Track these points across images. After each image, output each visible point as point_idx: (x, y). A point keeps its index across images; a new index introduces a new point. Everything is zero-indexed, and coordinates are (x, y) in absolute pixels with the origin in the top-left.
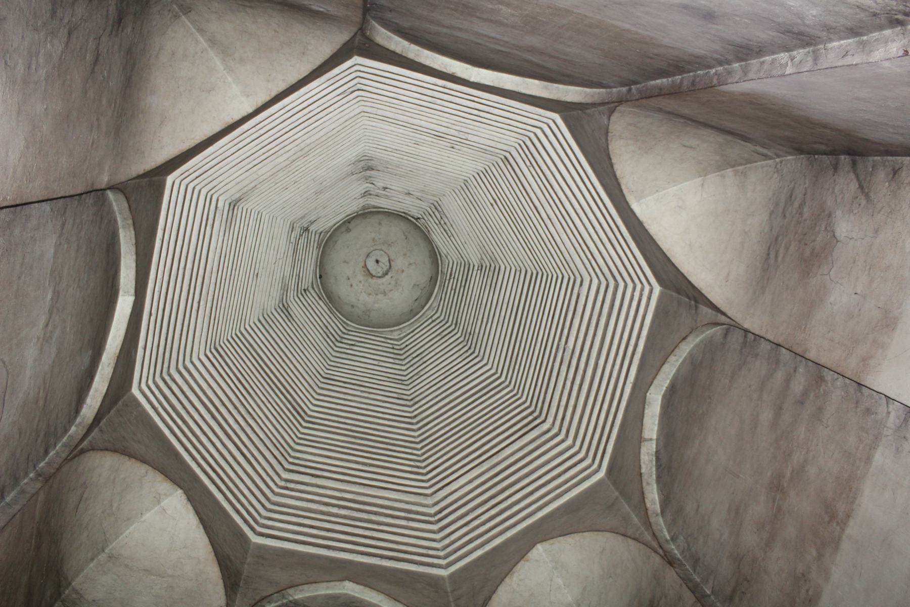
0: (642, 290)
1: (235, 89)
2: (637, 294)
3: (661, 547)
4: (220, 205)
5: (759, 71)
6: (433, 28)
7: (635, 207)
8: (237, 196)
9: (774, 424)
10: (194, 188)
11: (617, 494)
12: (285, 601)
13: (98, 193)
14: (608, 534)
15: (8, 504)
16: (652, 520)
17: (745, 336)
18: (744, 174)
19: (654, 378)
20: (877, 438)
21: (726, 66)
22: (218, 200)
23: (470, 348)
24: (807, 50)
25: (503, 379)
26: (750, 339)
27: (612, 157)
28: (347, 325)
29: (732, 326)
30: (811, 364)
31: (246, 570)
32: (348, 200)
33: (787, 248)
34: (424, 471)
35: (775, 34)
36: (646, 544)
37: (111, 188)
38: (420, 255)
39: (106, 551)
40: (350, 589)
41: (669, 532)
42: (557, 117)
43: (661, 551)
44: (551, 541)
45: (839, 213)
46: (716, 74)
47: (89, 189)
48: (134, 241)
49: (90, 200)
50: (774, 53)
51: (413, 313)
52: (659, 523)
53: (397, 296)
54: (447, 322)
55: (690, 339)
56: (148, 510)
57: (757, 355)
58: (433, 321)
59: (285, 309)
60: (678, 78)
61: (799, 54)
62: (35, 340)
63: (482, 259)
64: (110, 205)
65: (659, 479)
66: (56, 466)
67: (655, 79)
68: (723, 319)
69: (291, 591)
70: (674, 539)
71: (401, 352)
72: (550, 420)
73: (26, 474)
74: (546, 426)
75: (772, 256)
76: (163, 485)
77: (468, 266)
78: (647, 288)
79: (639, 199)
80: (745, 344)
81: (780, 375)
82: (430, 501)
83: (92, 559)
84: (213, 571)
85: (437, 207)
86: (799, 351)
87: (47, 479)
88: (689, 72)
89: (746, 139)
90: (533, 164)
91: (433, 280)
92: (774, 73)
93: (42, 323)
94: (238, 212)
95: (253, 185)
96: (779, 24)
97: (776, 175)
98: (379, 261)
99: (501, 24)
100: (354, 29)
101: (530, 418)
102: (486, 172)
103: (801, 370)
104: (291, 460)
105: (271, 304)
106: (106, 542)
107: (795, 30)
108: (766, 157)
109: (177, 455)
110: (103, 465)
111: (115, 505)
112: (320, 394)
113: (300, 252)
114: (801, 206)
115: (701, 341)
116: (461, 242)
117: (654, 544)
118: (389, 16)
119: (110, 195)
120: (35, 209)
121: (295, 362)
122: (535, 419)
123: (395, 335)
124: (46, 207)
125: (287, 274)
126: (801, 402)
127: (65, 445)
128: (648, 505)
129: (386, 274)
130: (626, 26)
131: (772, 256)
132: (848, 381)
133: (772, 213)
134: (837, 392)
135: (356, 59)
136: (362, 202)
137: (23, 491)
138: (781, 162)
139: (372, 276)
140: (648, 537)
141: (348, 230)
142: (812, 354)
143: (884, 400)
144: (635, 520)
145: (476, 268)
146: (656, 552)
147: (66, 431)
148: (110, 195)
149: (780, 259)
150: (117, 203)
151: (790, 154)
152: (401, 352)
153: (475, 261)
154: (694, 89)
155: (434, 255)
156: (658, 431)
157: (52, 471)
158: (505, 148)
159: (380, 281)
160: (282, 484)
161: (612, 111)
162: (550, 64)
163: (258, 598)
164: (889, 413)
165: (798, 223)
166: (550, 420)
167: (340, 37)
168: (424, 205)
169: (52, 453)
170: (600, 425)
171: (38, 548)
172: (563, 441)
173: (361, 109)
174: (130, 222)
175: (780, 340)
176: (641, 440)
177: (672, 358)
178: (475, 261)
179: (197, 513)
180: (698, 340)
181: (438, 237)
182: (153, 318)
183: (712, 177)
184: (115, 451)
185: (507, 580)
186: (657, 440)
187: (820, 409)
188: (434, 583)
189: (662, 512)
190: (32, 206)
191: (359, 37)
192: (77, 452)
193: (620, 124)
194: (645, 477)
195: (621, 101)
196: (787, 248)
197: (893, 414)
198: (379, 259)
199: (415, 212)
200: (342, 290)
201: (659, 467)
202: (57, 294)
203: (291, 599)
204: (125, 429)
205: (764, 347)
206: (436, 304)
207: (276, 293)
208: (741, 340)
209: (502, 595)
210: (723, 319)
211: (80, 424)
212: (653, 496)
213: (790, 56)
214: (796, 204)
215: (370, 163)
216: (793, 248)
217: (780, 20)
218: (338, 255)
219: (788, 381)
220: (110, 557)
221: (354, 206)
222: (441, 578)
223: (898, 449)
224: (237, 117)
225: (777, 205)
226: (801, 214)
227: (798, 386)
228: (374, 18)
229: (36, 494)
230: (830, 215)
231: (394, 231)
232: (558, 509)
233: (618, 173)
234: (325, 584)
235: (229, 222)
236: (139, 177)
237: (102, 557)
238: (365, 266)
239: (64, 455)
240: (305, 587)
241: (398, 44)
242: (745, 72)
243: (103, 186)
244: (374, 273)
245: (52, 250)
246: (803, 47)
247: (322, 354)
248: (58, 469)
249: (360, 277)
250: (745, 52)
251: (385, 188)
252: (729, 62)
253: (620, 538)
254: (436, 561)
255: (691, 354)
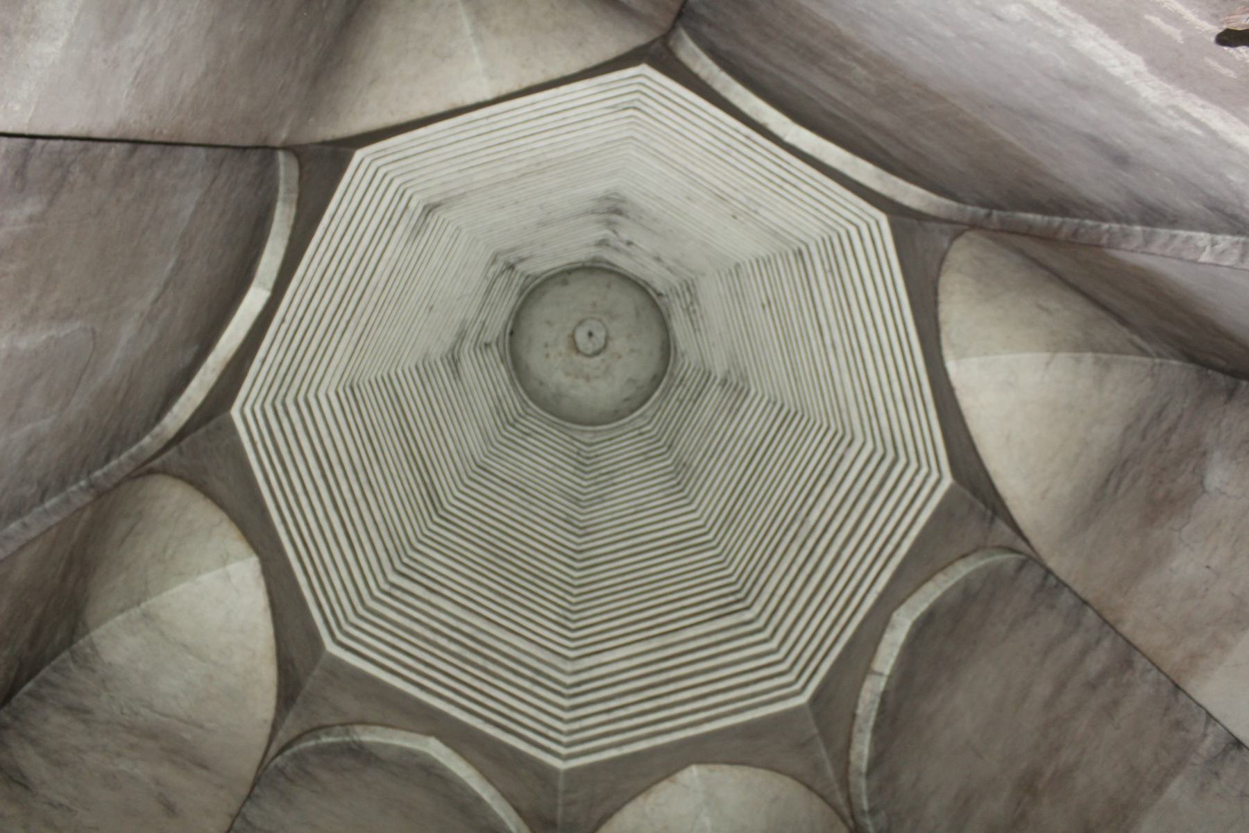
0: (928, 475)
1: (478, 64)
2: (919, 480)
3: (853, 817)
4: (413, 204)
5: (1165, 245)
6: (758, 61)
7: (951, 366)
8: (437, 200)
9: (1049, 704)
10: (385, 175)
11: (815, 731)
12: (347, 739)
13: (267, 151)
14: (788, 780)
15: (46, 511)
16: (852, 778)
17: (1045, 578)
18: (1107, 366)
19: (909, 595)
20: (1180, 763)
21: (1124, 226)
22: (410, 198)
23: (679, 484)
24: (1236, 238)
25: (710, 537)
26: (1050, 584)
27: (941, 291)
28: (528, 406)
29: (1031, 559)
30: (1120, 640)
31: (309, 684)
32: (578, 244)
33: (1134, 480)
34: (572, 626)
35: (1200, 207)
36: (834, 807)
37: (286, 148)
38: (649, 344)
39: (143, 605)
40: (434, 749)
41: (870, 800)
42: (883, 219)
43: (851, 822)
44: (711, 767)
45: (1217, 455)
46: (1108, 231)
47: (260, 143)
48: (291, 222)
49: (255, 157)
50: (1191, 228)
51: (617, 415)
52: (861, 785)
53: (603, 389)
54: (659, 441)
55: (971, 559)
56: (208, 570)
57: (1052, 607)
58: (641, 434)
59: (453, 361)
60: (1057, 220)
61: (1225, 241)
62: (137, 316)
63: (729, 372)
64: (276, 170)
65: (877, 728)
66: (115, 480)
67: (1026, 211)
68: (1022, 546)
69: (358, 729)
70: (873, 812)
71: (587, 462)
72: (757, 608)
73: (77, 480)
74: (748, 615)
75: (1113, 483)
76: (230, 540)
77: (707, 375)
78: (935, 476)
79: (961, 355)
80: (1041, 587)
81: (1076, 642)
82: (569, 667)
83: (122, 611)
84: (268, 674)
85: (690, 288)
86: (1110, 618)
87: (102, 495)
88: (1074, 216)
89: (1123, 321)
90: (833, 270)
91: (656, 380)
92: (1184, 254)
93: (152, 294)
94: (432, 220)
95: (462, 191)
96: (1209, 197)
97: (1149, 380)
98: (593, 335)
99: (848, 85)
100: (655, 34)
101: (731, 599)
102: (768, 262)
103: (1106, 643)
104: (406, 560)
105: (438, 350)
106: (145, 595)
107: (1229, 210)
108: (1143, 352)
109: (264, 510)
110: (172, 499)
111: (170, 552)
112: (467, 486)
113: (494, 293)
114: (1171, 430)
115: (986, 567)
116: (705, 343)
117: (846, 811)
118: (705, 29)
119: (281, 156)
120: (187, 153)
121: (447, 434)
122: (737, 601)
123: (586, 438)
124: (202, 152)
125: (470, 316)
126: (1092, 686)
127: (132, 458)
128: (853, 757)
129: (597, 353)
130: (1010, 138)
131: (1113, 483)
132: (1163, 678)
133: (1128, 428)
134: (1144, 687)
135: (644, 69)
136: (594, 252)
137: (67, 501)
138: (1161, 365)
139: (578, 351)
140: (840, 799)
141: (565, 283)
142: (1125, 629)
143: (1203, 717)
144: (830, 772)
145: (718, 381)
146: (844, 821)
147: (138, 438)
148: (281, 156)
149: (1121, 491)
150: (286, 169)
151: (1176, 358)
152: (587, 462)
153: (719, 372)
154: (1072, 243)
155: (667, 349)
156: (894, 666)
157: (109, 485)
158: (803, 237)
159: (586, 361)
160: (386, 587)
161: (958, 235)
162: (896, 152)
163: (315, 724)
164: (1205, 735)
165: (1160, 451)
166: (757, 608)
167: (635, 38)
168: (674, 280)
169: (114, 463)
170: (818, 638)
171: (64, 578)
172: (765, 641)
173: (630, 133)
174: (295, 196)
175: (1089, 596)
176: (868, 670)
177: (940, 577)
178: (719, 372)
179: (270, 592)
180: (982, 563)
181: (680, 326)
182: (285, 326)
183: (1064, 358)
184: (191, 482)
185: (640, 799)
186: (890, 677)
187: (1116, 703)
188: (544, 774)
189: (869, 773)
190: (186, 148)
191: (657, 45)
192: (145, 470)
193: (962, 253)
194: (859, 721)
195: (974, 225)
196: (1134, 480)
197: (1209, 741)
198: (594, 332)
199: (659, 285)
200: (536, 360)
201: (882, 711)
202: (180, 264)
203: (356, 738)
204: (210, 461)
205: (1066, 600)
206: (650, 413)
207: (448, 339)
208: (1038, 581)
209: (628, 816)
210: (1022, 546)
211: (157, 435)
212: (862, 748)
213: (1212, 240)
214: (1165, 426)
215: (621, 206)
216: (1142, 483)
217: (1212, 193)
218: (544, 311)
219: (1084, 653)
220: (145, 615)
221: (580, 253)
222: (553, 771)
223: (1202, 785)
224: (469, 100)
225: (1138, 419)
226: (1167, 441)
227: (1095, 663)
228: (686, 28)
229: (81, 509)
230: (1204, 454)
231: (626, 301)
232: (732, 728)
233: (942, 316)
234: (403, 733)
235: (417, 231)
236: (324, 143)
237: (135, 612)
238: (573, 336)
239: (128, 470)
240: (379, 729)
241: (705, 67)
242: (1148, 241)
243: (277, 144)
244: (581, 347)
245: (191, 208)
246: (1233, 233)
247: (487, 440)
248: (117, 485)
249: (563, 347)
250: (1155, 216)
251: (629, 243)
252: (1129, 222)
253: (803, 789)
254: (554, 746)
255: (966, 579)
